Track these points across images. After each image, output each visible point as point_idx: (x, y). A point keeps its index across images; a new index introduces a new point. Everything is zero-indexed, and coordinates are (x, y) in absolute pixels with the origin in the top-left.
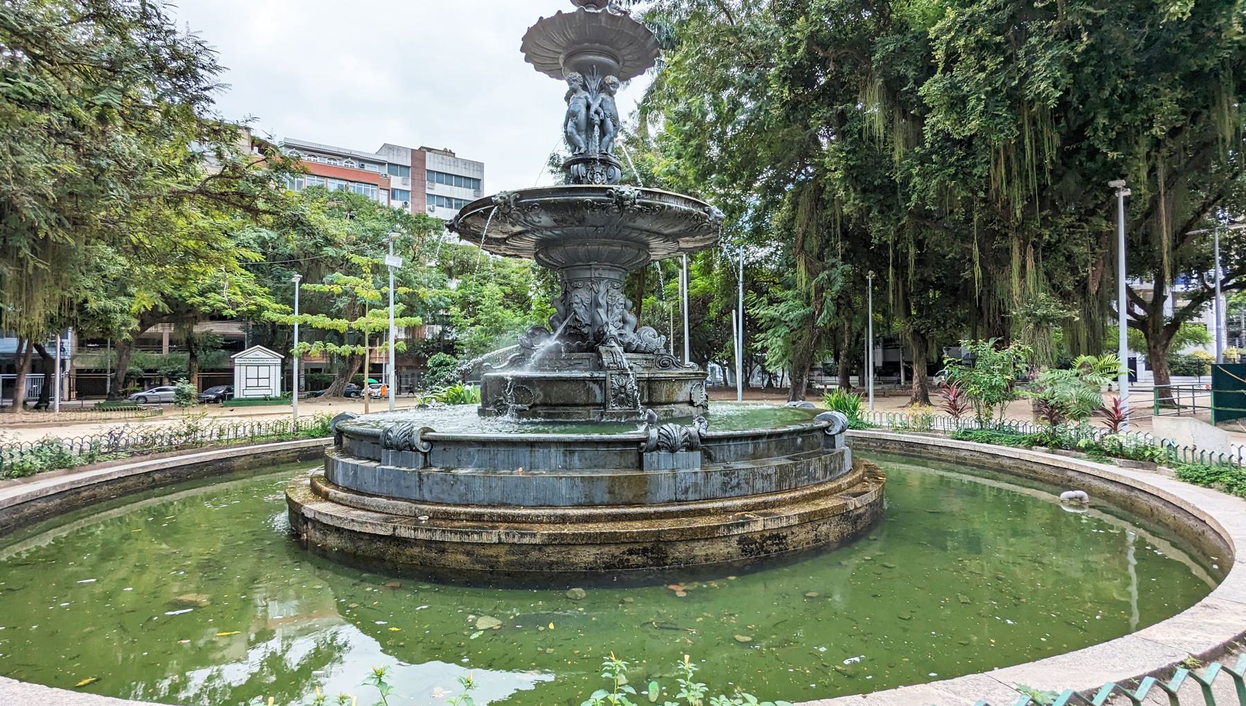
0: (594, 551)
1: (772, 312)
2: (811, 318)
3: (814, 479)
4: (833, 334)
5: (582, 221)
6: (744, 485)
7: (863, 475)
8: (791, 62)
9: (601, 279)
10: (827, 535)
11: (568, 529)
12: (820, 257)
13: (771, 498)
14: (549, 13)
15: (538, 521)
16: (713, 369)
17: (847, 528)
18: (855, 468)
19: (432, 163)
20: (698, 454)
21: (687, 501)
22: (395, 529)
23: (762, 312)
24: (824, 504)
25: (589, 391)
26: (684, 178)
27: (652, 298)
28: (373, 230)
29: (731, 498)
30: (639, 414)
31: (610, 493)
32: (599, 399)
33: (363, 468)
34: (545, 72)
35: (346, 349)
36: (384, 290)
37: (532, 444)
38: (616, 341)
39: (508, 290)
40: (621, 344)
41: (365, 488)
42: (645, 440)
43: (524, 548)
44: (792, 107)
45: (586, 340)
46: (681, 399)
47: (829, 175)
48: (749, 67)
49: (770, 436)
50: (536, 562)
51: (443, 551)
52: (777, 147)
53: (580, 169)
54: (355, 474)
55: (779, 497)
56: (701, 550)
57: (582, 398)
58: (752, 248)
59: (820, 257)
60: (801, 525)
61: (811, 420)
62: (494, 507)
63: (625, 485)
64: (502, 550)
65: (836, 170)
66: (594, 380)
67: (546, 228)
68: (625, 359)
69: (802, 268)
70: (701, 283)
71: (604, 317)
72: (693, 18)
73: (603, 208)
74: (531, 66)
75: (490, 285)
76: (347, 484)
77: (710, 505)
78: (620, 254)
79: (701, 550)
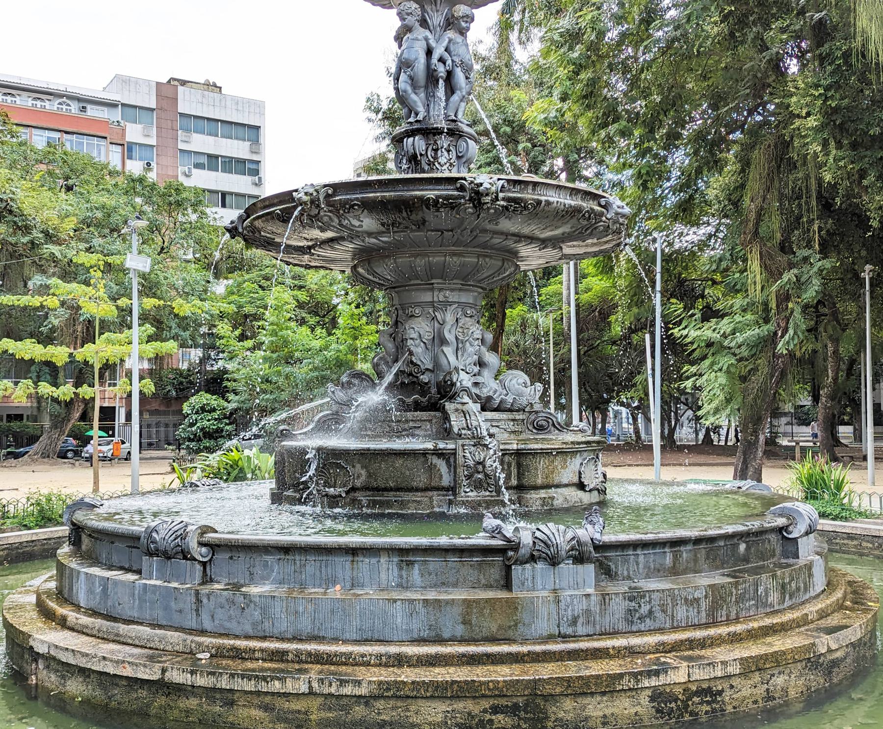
1: (708, 332)
2: (772, 340)
3: (765, 605)
4: (807, 366)
5: (422, 224)
6: (659, 615)
7: (844, 598)
9: (447, 304)
10: (785, 691)
11: (408, 675)
12: (785, 247)
13: (699, 634)
16: (617, 414)
17: (817, 680)
18: (830, 586)
19: (188, 103)
20: (590, 568)
21: (575, 637)
22: (164, 671)
23: (693, 334)
24: (778, 644)
25: (432, 468)
26: (573, 129)
27: (520, 309)
29: (640, 633)
30: (503, 504)
31: (464, 623)
32: (446, 480)
33: (116, 583)
35: (66, 391)
36: (123, 302)
37: (353, 551)
38: (470, 395)
39: (303, 296)
40: (477, 398)
41: (118, 611)
43: (345, 701)
46: (565, 481)
47: (797, 123)
49: (698, 541)
51: (232, 703)
52: (717, 79)
53: (418, 144)
54: (105, 590)
55: (712, 632)
57: (421, 480)
58: (679, 227)
59: (785, 247)
60: (744, 675)
62: (301, 640)
63: (487, 611)
65: (808, 114)
66: (439, 454)
67: (370, 234)
68: (481, 421)
69: (755, 265)
70: (597, 284)
71: (452, 358)
73: (452, 207)
76: (93, 604)
78: (477, 269)
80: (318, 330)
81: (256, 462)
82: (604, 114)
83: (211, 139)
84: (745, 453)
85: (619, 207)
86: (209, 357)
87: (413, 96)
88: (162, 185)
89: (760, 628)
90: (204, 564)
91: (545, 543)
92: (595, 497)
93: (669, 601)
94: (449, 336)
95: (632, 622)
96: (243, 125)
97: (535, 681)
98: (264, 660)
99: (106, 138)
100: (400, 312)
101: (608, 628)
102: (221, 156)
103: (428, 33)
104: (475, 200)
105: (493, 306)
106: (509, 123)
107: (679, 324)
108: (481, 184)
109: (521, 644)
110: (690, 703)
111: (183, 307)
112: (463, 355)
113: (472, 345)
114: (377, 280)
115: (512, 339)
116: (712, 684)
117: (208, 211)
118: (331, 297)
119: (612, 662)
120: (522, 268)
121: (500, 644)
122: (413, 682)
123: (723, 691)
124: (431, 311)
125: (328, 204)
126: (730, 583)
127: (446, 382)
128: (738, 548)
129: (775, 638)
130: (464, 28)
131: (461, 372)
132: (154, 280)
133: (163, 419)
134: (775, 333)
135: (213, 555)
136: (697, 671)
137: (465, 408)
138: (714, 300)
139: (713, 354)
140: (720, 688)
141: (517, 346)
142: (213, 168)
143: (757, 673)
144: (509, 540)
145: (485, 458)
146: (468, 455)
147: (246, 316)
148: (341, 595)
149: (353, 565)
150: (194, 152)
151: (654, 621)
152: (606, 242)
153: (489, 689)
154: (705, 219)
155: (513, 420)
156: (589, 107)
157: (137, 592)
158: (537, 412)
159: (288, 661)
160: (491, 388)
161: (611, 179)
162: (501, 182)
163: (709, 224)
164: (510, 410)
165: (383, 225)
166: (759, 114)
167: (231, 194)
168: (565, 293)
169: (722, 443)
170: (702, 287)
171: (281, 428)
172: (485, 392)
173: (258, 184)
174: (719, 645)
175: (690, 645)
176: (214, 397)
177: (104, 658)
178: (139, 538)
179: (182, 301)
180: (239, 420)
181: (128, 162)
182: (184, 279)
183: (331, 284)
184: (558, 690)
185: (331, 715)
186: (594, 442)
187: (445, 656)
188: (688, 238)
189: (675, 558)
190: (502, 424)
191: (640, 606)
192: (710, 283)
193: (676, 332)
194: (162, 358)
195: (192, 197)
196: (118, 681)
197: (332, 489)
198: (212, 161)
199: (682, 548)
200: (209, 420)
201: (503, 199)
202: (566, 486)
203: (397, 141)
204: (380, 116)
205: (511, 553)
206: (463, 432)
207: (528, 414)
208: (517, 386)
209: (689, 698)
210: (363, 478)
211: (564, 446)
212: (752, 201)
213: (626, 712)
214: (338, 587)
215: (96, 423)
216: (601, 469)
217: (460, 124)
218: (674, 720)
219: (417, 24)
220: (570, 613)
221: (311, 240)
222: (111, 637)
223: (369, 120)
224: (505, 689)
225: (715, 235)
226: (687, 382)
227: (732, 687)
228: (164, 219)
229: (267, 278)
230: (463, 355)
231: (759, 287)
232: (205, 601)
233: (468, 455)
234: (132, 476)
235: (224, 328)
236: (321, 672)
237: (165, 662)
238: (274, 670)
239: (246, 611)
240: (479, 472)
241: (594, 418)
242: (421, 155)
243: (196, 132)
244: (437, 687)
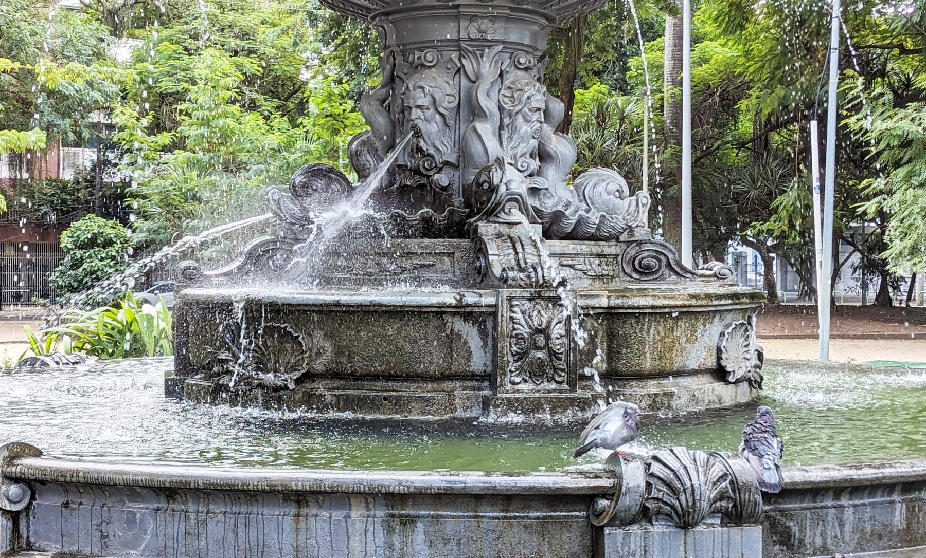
9: (483, 44)
16: (739, 259)
20: (755, 533)
23: (880, 126)
25: (452, 341)
32: (479, 361)
37: (298, 498)
38: (523, 208)
39: (252, 66)
40: (536, 215)
42: (612, 493)
46: (693, 364)
57: (435, 360)
68: (549, 259)
70: (722, 52)
71: (492, 144)
75: (209, 55)
90: (14, 517)
91: (669, 485)
92: (743, 394)
94: (488, 104)
100: (399, 60)
112: (510, 138)
113: (526, 121)
124: (454, 56)
127: (479, 185)
131: (507, 166)
132: (16, 36)
135: (33, 498)
137: (515, 232)
139: (910, 161)
145: (549, 323)
149: (297, 522)
155: (600, 256)
158: (640, 243)
164: (594, 238)
168: (668, 64)
170: (882, 59)
171: (184, 264)
172: (549, 205)
176: (110, 223)
190: (578, 262)
192: (896, 51)
197: (271, 375)
202: (694, 373)
205: (603, 503)
206: (511, 274)
207: (624, 246)
208: (605, 196)
210: (328, 356)
211: (694, 302)
216: (755, 343)
226: (868, 204)
229: (196, 37)
230: (510, 138)
233: (519, 316)
235: (125, 115)
240: (539, 348)
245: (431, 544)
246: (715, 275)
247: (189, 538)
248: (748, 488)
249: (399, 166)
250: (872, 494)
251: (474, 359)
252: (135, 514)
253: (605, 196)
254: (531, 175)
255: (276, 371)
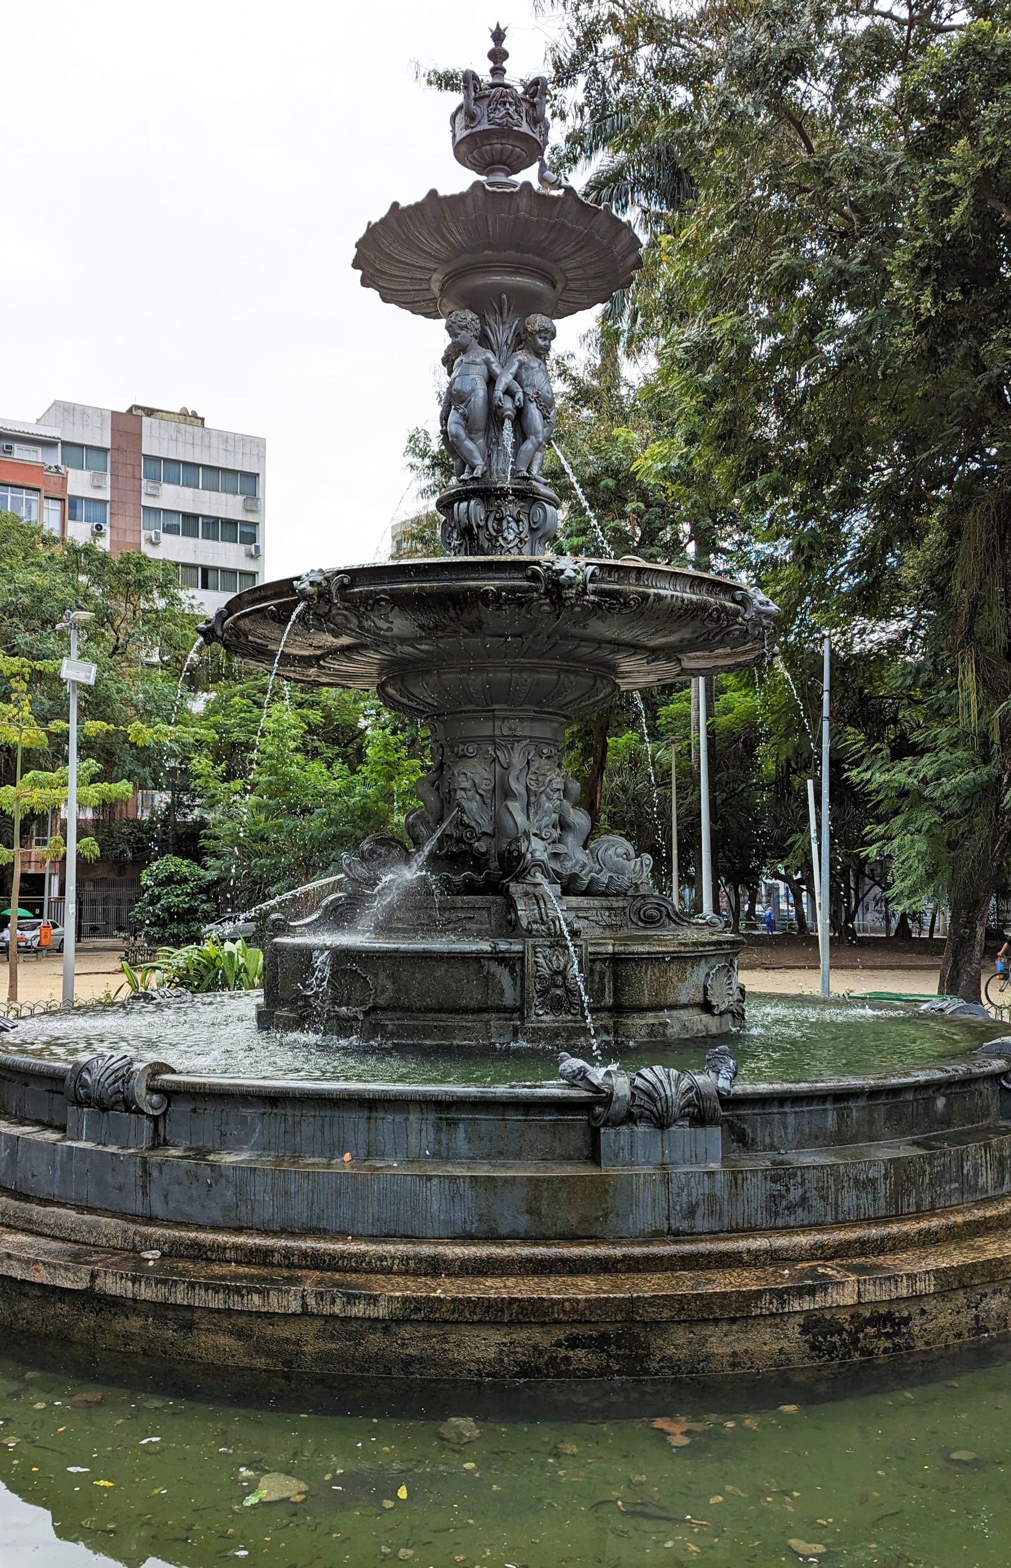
0: (496, 1337)
1: (901, 775)
3: (975, 1189)
5: (476, 627)
6: (816, 1202)
8: (939, 234)
11: (445, 1289)
14: (411, 196)
15: (382, 1268)
16: (772, 890)
19: (155, 441)
20: (716, 1132)
21: (692, 1235)
22: (94, 1276)
23: (880, 778)
25: (488, 980)
27: (629, 736)
28: (33, 588)
29: (788, 1230)
31: (529, 1212)
32: (510, 997)
33: (30, 1144)
34: (402, 304)
36: (56, 725)
37: (370, 1104)
38: (545, 873)
39: (316, 716)
40: (554, 877)
43: (353, 1327)
44: (939, 331)
45: (480, 871)
46: (684, 999)
48: (842, 239)
49: (874, 1093)
50: (378, 1358)
51: (189, 1326)
53: (473, 510)
54: (13, 1155)
55: (894, 1229)
56: (721, 1343)
57: (474, 996)
58: (860, 622)
60: (943, 1293)
61: (967, 1055)
62: (292, 1234)
63: (563, 1195)
64: (310, 1328)
67: (403, 640)
68: (560, 909)
69: (969, 679)
70: (740, 701)
71: (520, 819)
72: (720, 143)
74: (373, 294)
77: (742, 1245)
79: (721, 1343)
80: (337, 766)
81: (242, 960)
82: (749, 461)
83: (189, 491)
84: (955, 954)
85: (761, 603)
86: (180, 804)
87: (469, 444)
88: (116, 558)
89: (966, 1224)
93: (831, 1182)
95: (777, 1213)
96: (235, 472)
97: (631, 1300)
98: (239, 1263)
99: (38, 490)
101: (740, 1221)
102: (203, 516)
103: (490, 355)
104: (553, 593)
105: (589, 733)
106: (613, 472)
107: (857, 763)
108: (562, 571)
109: (613, 1244)
110: (861, 1335)
111: (141, 733)
112: (536, 813)
113: (549, 799)
114: (414, 704)
115: (617, 780)
116: (894, 1308)
117: (181, 594)
118: (357, 719)
119: (746, 1274)
120: (623, 688)
121: (582, 1245)
122: (454, 1300)
123: (909, 1318)
125: (344, 599)
126: (922, 1156)
127: (510, 852)
128: (934, 1104)
129: (988, 1240)
130: (541, 348)
131: (532, 837)
132: (103, 693)
133: (113, 892)
134: (999, 779)
135: (169, 1105)
136: (872, 1288)
137: (538, 891)
138: (911, 727)
140: (906, 1314)
141: (624, 791)
142: (190, 532)
143: (961, 1292)
144: (596, 1089)
145: (566, 966)
146: (541, 960)
147: (233, 745)
148: (352, 1168)
150: (165, 510)
151: (809, 1212)
152: (745, 653)
153: (565, 1312)
154: (898, 609)
155: (608, 909)
156: (727, 451)
157: (58, 1158)
158: (644, 897)
159: (272, 1265)
160: (577, 862)
161: (751, 558)
162: (591, 568)
163: (903, 617)
164: (604, 894)
165: (421, 627)
166: (975, 460)
167: (216, 569)
169: (925, 935)
170: (894, 707)
172: (569, 867)
173: (255, 556)
174: (905, 1250)
175: (862, 1249)
176: (186, 862)
177: (9, 1256)
178: (63, 1080)
179: (140, 725)
180: (219, 898)
181: (70, 524)
182: (145, 692)
183: (355, 701)
184: (666, 1314)
185: (334, 1346)
186: (726, 942)
187: (502, 1260)
188: (874, 637)
189: (841, 1117)
190: (592, 915)
191: (788, 1190)
193: (853, 774)
194: (112, 806)
195: (160, 575)
196: (26, 1289)
198: (190, 523)
199: (851, 1104)
200: (178, 896)
201: (594, 592)
202: (685, 1006)
203: (444, 507)
204: (427, 461)
205: (599, 1110)
207: (630, 900)
208: (615, 859)
209: (860, 1329)
211: (682, 949)
212: (964, 587)
213: (766, 1348)
214: (347, 1157)
215: (15, 897)
217: (534, 483)
218: (837, 1361)
219: (474, 341)
220: (685, 1199)
221: (320, 647)
222: (21, 1224)
223: (412, 467)
224: (587, 1312)
225: (912, 633)
227: (923, 1312)
228: (119, 606)
230: (536, 813)
231: (974, 711)
232: (155, 1173)
233: (541, 960)
234: (64, 976)
235: (201, 763)
236: (320, 1282)
237: (95, 1263)
238: (251, 1278)
239: (215, 1188)
240: (557, 987)
241: (737, 896)
242: (479, 526)
243: (167, 481)
244: (488, 1307)
245: (470, 1141)
246: (707, 924)
247: (288, 1136)
248: (708, 1097)
249: (447, 835)
250: (809, 1104)
251: (506, 995)
252: (246, 1117)
253: (615, 859)
254: (554, 842)
255: (347, 1005)
